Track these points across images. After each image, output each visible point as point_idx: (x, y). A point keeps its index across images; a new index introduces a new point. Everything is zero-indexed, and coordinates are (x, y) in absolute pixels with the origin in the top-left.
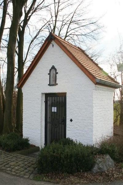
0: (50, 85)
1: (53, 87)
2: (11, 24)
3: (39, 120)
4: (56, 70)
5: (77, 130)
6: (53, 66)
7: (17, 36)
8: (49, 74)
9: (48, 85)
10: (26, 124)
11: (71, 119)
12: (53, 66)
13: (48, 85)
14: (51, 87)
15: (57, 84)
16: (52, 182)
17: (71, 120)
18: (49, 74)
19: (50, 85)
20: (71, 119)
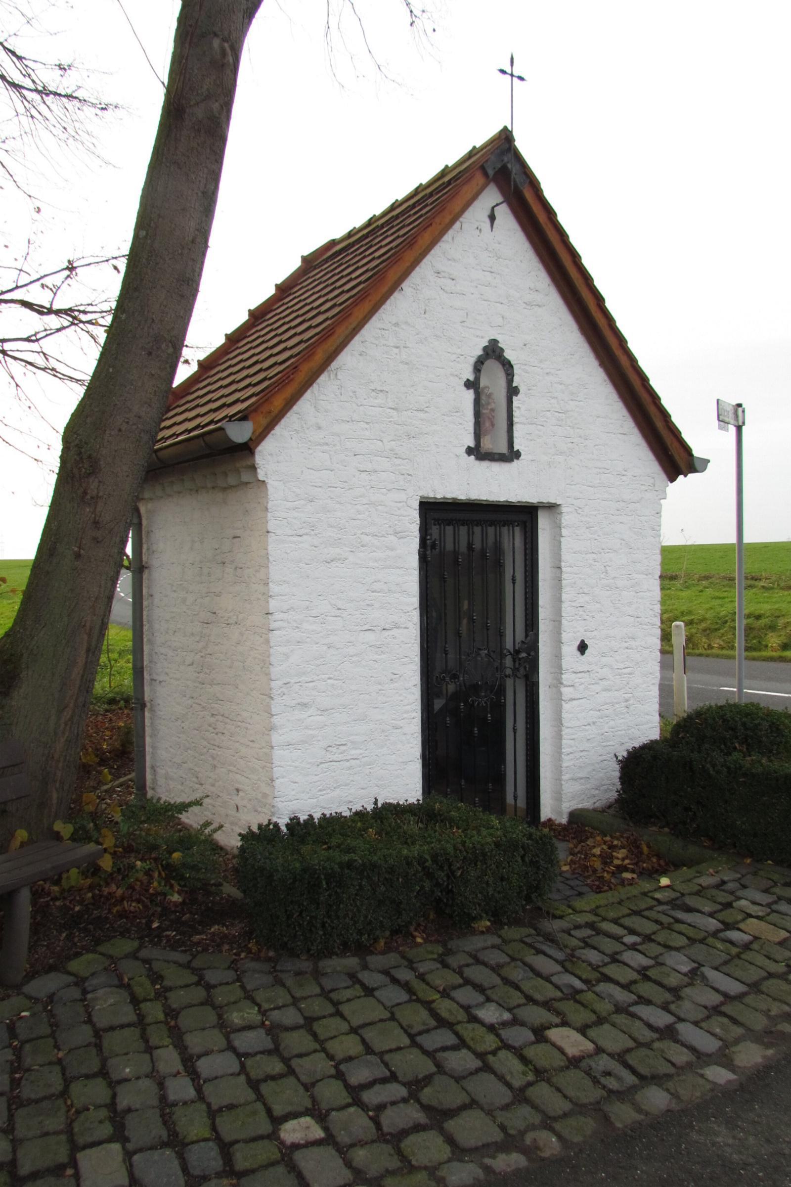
0: (477, 452)
1: (496, 468)
2: (61, 447)
3: (567, 578)
4: (508, 367)
5: (605, 690)
6: (494, 343)
7: (127, 541)
8: (468, 384)
9: (470, 451)
10: (569, 569)
11: (583, 642)
12: (494, 343)
13: (470, 451)
14: (485, 464)
15: (517, 455)
16: (500, 604)
17: (583, 648)
18: (468, 384)
19: (477, 452)
20: (583, 642)
